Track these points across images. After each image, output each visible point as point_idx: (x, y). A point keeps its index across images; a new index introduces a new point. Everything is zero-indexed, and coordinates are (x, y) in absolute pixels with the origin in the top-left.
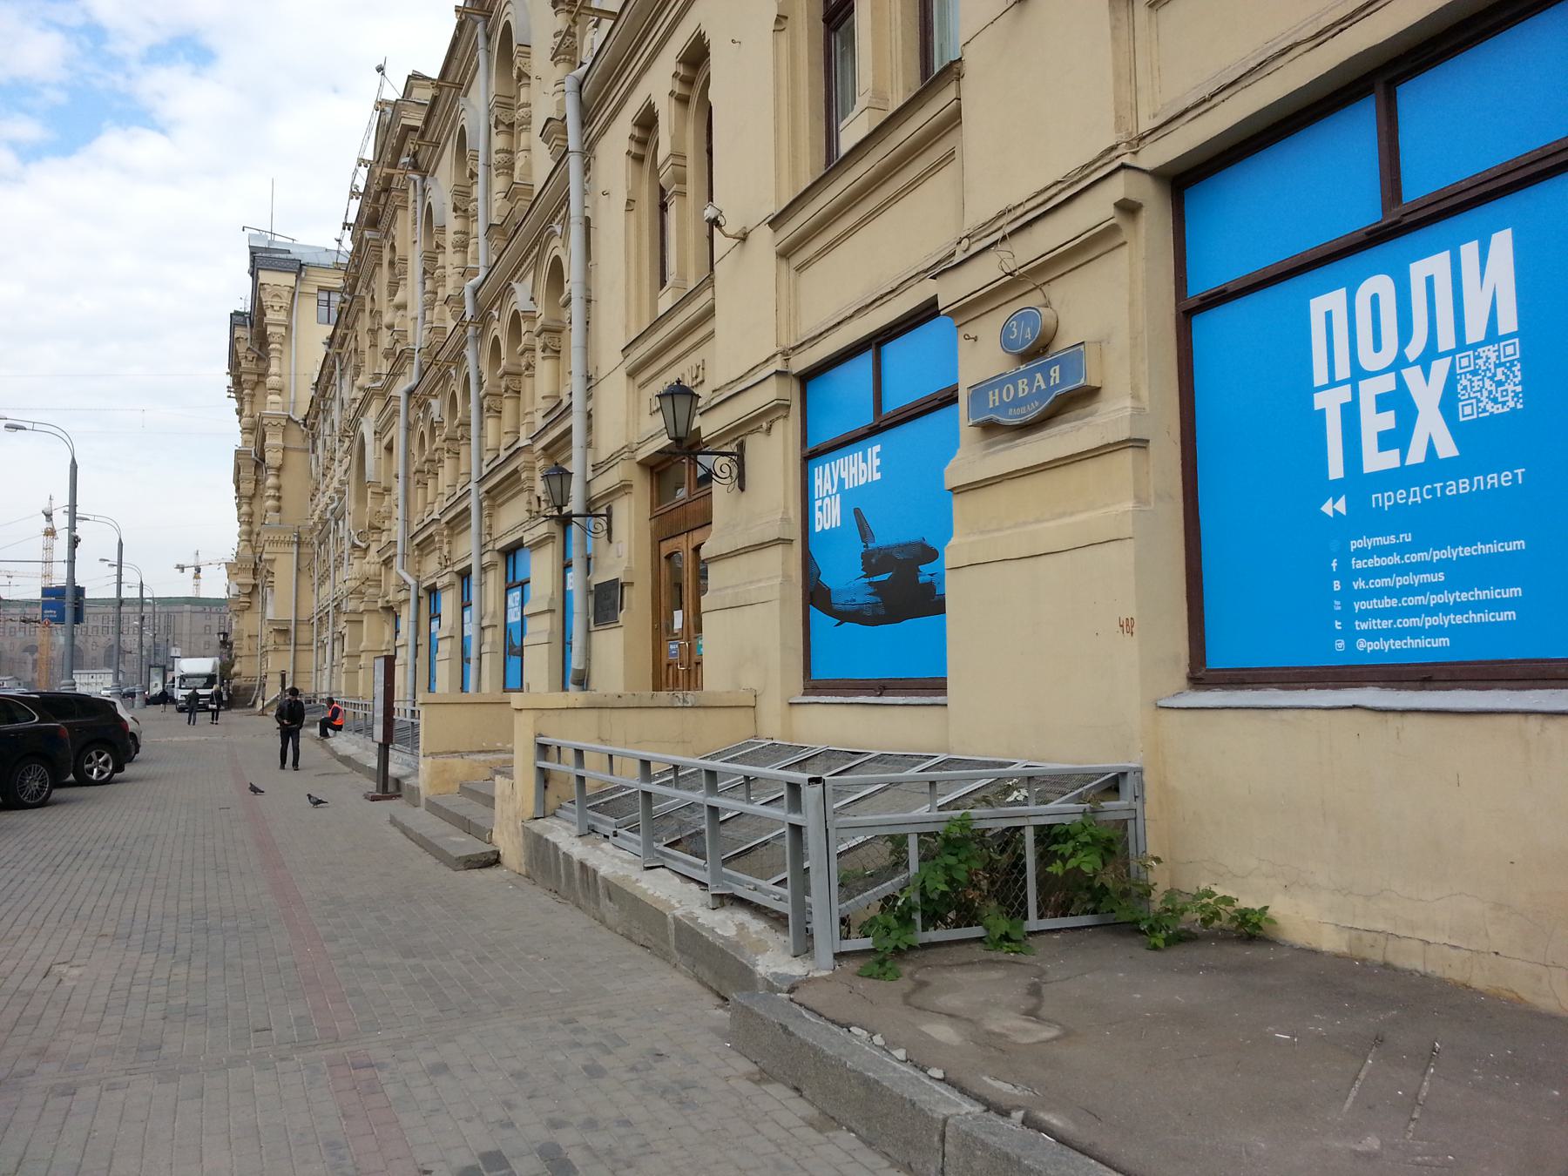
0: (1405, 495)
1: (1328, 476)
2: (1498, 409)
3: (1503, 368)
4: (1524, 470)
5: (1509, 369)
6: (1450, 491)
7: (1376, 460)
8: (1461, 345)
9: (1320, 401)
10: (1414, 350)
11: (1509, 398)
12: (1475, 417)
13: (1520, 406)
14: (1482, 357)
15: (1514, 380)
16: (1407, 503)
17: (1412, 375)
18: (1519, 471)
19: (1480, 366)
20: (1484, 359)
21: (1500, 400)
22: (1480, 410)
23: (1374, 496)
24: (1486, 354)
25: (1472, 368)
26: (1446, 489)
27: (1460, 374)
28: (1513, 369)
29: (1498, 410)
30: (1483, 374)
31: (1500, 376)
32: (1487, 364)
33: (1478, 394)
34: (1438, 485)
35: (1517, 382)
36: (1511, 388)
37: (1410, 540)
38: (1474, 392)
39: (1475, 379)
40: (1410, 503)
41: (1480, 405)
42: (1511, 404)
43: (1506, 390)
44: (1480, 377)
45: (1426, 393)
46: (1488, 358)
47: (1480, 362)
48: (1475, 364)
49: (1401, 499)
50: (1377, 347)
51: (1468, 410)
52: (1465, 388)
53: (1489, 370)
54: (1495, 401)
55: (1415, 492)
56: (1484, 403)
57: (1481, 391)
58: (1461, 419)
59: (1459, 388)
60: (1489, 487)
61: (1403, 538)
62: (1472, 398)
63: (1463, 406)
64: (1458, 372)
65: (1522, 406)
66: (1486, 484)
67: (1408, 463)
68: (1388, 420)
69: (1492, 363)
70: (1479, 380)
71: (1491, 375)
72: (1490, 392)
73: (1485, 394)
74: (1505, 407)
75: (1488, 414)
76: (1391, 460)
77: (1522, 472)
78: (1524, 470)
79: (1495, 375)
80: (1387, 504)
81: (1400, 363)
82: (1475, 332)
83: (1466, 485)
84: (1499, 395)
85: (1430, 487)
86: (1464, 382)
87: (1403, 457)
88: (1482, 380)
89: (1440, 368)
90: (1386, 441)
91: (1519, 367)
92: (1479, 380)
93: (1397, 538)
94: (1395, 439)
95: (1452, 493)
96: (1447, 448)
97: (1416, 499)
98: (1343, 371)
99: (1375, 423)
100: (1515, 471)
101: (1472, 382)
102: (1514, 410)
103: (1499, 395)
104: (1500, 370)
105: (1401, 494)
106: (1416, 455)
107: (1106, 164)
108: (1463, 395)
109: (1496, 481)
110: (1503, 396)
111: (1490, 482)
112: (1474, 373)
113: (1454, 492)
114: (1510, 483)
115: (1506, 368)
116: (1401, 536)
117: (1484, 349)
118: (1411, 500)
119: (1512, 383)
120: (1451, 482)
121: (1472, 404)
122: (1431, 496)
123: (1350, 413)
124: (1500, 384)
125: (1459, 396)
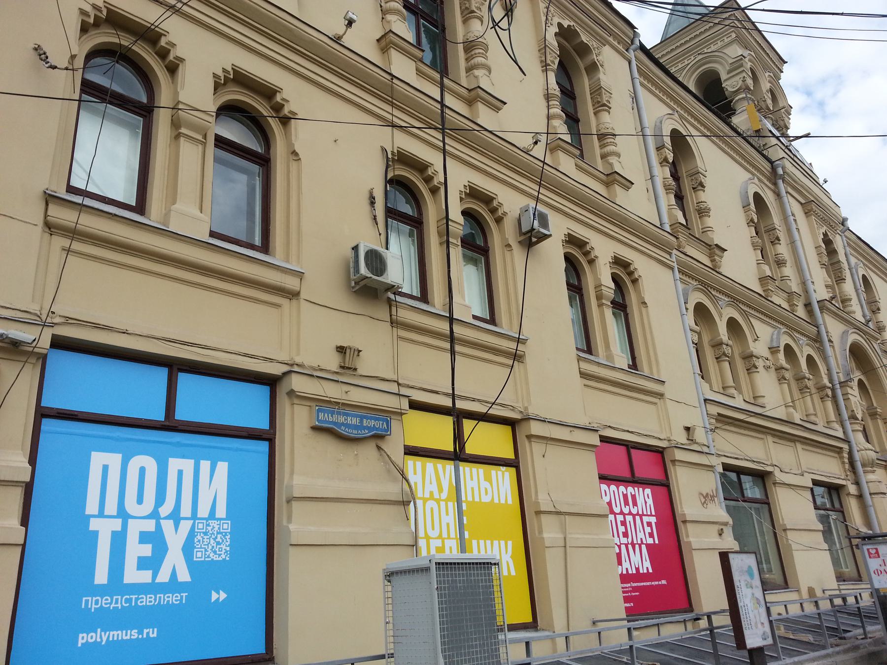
0: (109, 601)
1: (94, 581)
2: (216, 557)
3: (221, 535)
4: (187, 594)
5: (224, 536)
6: (142, 602)
7: (133, 575)
8: (194, 516)
9: (95, 524)
10: (166, 509)
11: (223, 553)
12: (203, 559)
13: (228, 559)
14: (210, 526)
15: (226, 543)
16: (110, 607)
17: (167, 526)
18: (184, 595)
19: (209, 531)
20: (212, 527)
21: (218, 553)
22: (206, 556)
23: (84, 599)
24: (213, 524)
25: (204, 530)
26: (138, 601)
27: (197, 532)
28: (226, 537)
29: (216, 558)
30: (210, 535)
31: (219, 539)
32: (213, 531)
33: (206, 547)
34: (134, 597)
35: (227, 545)
36: (224, 547)
37: (155, 635)
38: (204, 545)
39: (206, 537)
40: (111, 608)
41: (206, 553)
42: (223, 556)
43: (222, 548)
44: (208, 537)
45: (175, 539)
46: (214, 527)
47: (209, 528)
48: (206, 529)
49: (106, 604)
50: (140, 501)
51: (199, 555)
52: (199, 541)
53: (213, 533)
54: (215, 552)
55: (117, 599)
56: (209, 553)
57: (208, 545)
58: (195, 559)
59: (196, 540)
60: (165, 603)
61: (148, 633)
62: (203, 548)
63: (197, 551)
64: (196, 530)
65: (228, 559)
66: (164, 599)
67: (157, 581)
68: (146, 550)
69: (216, 531)
70: (207, 539)
71: (214, 537)
72: (213, 547)
73: (210, 547)
74: (220, 557)
75: (210, 559)
76: (145, 577)
77: (186, 595)
78: (187, 594)
79: (216, 538)
80: (94, 606)
81: (154, 515)
82: (203, 511)
83: (152, 600)
84: (217, 550)
85: (128, 597)
86: (199, 537)
87: (154, 576)
88: (209, 539)
89: (185, 526)
90: (143, 563)
91: (229, 537)
92: (207, 539)
93: (140, 632)
94: (151, 563)
95: (142, 604)
96: (184, 576)
97: (116, 606)
98: (111, 508)
99: (135, 550)
100: (182, 594)
101: (203, 539)
102: (224, 560)
103: (217, 550)
104: (219, 536)
105: (107, 600)
106: (164, 577)
107: (748, 390)
108: (198, 545)
109: (170, 599)
110: (219, 551)
111: (167, 599)
112: (205, 533)
113: (144, 603)
114: (178, 602)
115: (223, 535)
116: (145, 631)
117: (212, 521)
118: (113, 605)
119: (225, 545)
120: (143, 596)
121: (202, 551)
122: (128, 604)
123: (119, 540)
124: (218, 543)
125: (195, 545)
